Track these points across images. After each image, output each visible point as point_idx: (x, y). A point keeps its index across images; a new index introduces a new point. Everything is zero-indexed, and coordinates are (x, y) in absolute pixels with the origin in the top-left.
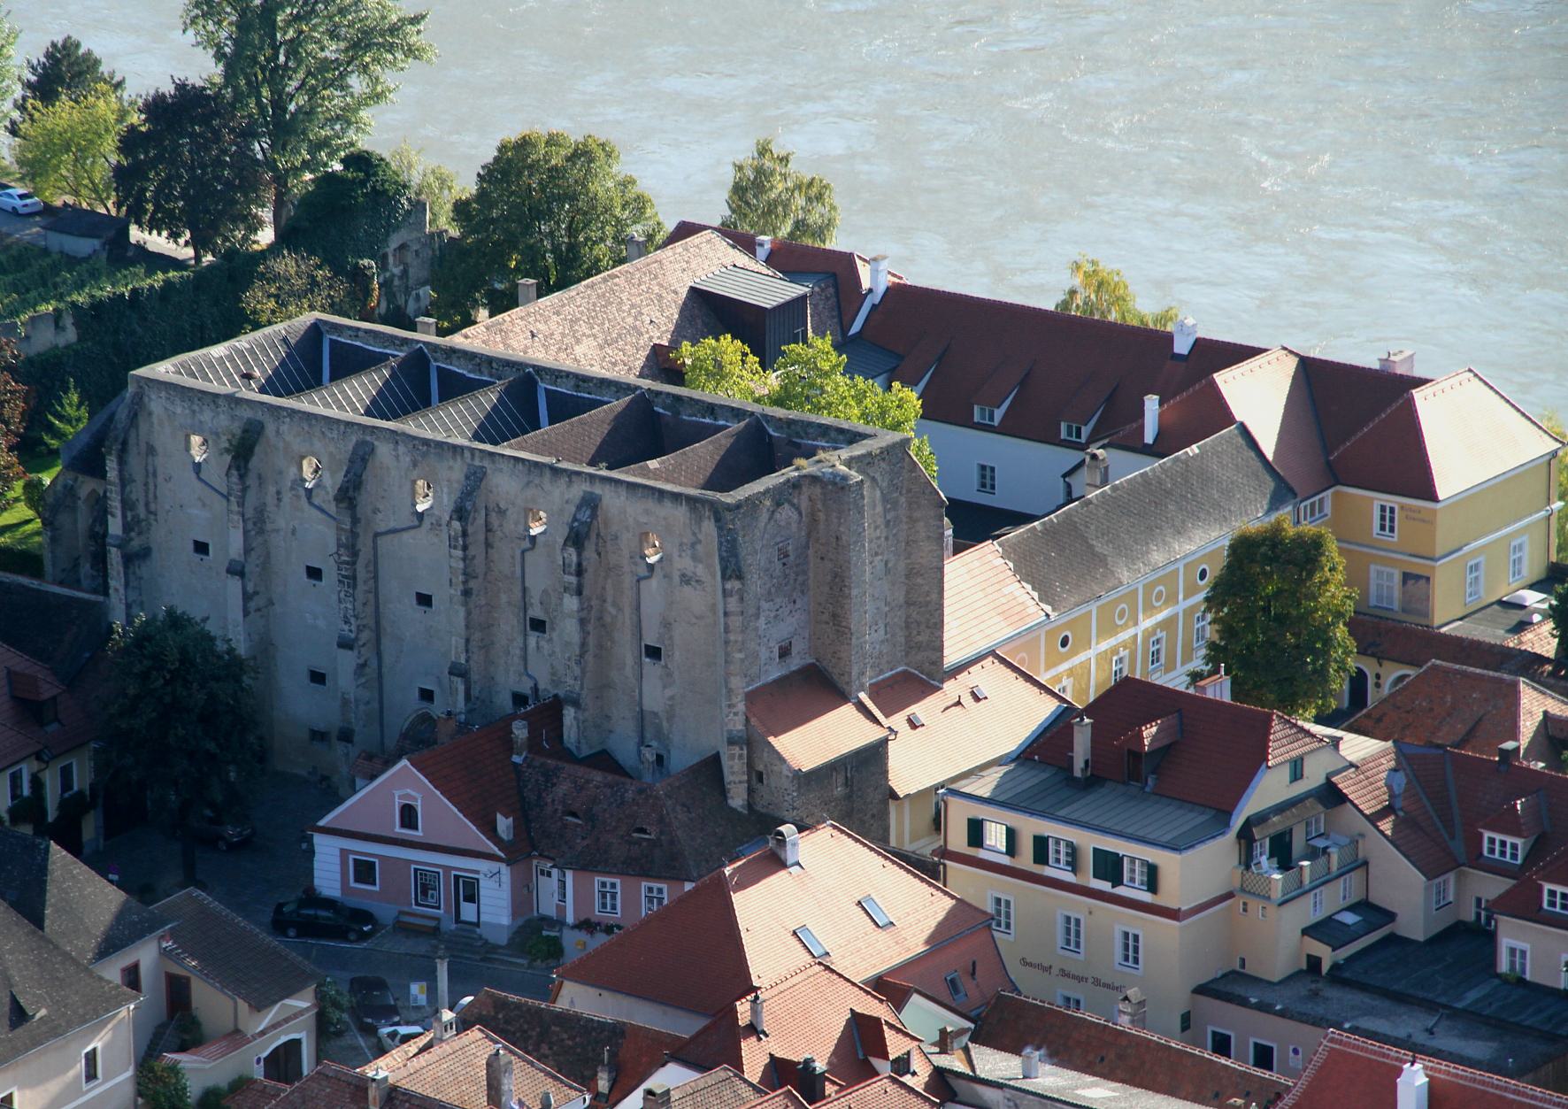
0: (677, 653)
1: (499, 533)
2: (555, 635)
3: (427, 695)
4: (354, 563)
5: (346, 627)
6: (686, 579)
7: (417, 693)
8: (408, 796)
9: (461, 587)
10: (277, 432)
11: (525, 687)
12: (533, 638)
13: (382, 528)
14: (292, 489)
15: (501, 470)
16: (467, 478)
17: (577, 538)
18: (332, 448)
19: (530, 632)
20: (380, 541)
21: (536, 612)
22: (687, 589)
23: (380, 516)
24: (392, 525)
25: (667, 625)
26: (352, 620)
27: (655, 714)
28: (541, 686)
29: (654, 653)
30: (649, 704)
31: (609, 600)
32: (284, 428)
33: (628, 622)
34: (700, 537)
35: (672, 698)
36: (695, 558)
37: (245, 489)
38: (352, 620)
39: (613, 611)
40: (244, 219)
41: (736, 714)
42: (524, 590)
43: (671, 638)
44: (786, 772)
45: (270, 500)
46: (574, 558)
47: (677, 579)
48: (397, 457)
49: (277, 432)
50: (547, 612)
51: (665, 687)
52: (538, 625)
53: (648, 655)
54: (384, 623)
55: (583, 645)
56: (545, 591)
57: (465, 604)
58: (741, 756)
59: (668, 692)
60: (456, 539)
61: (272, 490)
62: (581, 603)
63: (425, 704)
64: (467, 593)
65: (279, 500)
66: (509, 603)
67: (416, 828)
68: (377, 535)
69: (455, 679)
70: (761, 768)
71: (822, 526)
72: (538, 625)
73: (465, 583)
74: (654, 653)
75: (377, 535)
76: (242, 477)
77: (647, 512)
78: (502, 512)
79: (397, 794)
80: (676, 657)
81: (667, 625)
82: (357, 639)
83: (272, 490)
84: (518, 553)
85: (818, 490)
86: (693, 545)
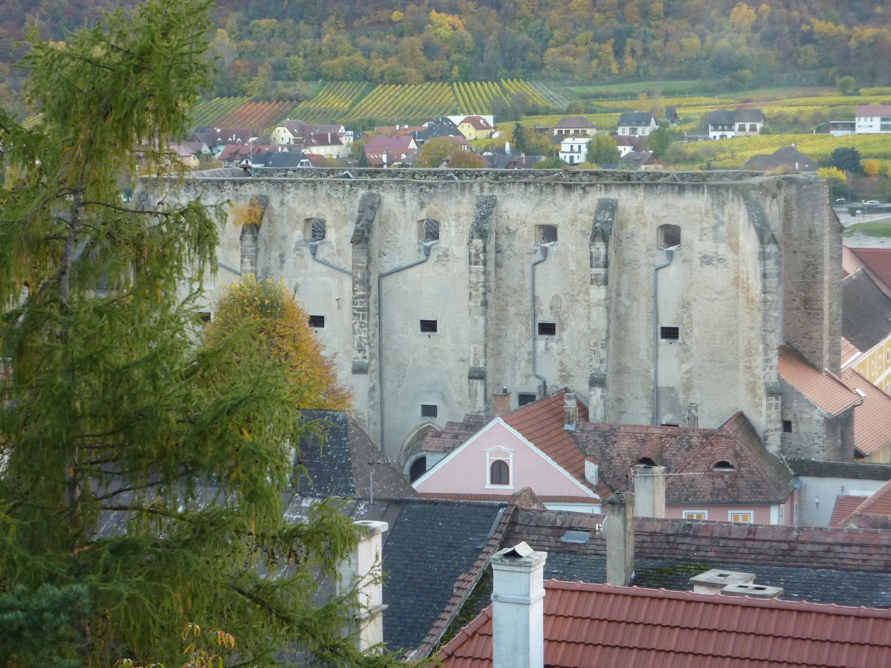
0: (696, 330)
1: (509, 253)
2: (565, 335)
3: (430, 411)
4: (368, 297)
5: (360, 355)
6: (706, 260)
7: (419, 410)
8: (500, 452)
9: (481, 298)
10: (282, 203)
11: (532, 387)
12: (542, 341)
13: (388, 268)
14: (296, 249)
15: (512, 196)
16: (479, 206)
17: (601, 234)
18: (337, 207)
19: (539, 337)
20: (384, 281)
21: (546, 317)
22: (708, 269)
23: (385, 258)
24: (397, 264)
25: (685, 305)
26: (367, 348)
27: (672, 389)
28: (549, 384)
29: (671, 333)
30: (663, 382)
31: (624, 293)
32: (289, 198)
33: (644, 311)
34: (722, 218)
35: (687, 372)
36: (716, 239)
37: (257, 251)
38: (367, 348)
39: (627, 302)
40: (8, 286)
41: (771, 368)
42: (534, 299)
43: (690, 317)
44: (816, 417)
45: (274, 263)
46: (603, 251)
47: (697, 262)
48: (404, 203)
49: (282, 203)
50: (557, 315)
51: (682, 362)
52: (547, 329)
53: (663, 337)
54: (388, 354)
55: (608, 331)
56: (556, 298)
57: (484, 314)
58: (776, 405)
59: (686, 367)
60: (477, 256)
61: (275, 254)
62: (609, 291)
63: (429, 419)
64: (485, 304)
65: (282, 262)
66: (518, 314)
67: (507, 483)
68: (382, 276)
69: (475, 381)
70: (789, 418)
71: (795, 223)
72: (547, 329)
73: (484, 294)
74: (671, 333)
75: (382, 276)
76: (255, 239)
77: (667, 206)
78: (510, 233)
79: (488, 451)
80: (694, 334)
81: (685, 305)
82: (369, 365)
83: (275, 254)
84: (528, 268)
85: (793, 191)
86: (715, 228)
